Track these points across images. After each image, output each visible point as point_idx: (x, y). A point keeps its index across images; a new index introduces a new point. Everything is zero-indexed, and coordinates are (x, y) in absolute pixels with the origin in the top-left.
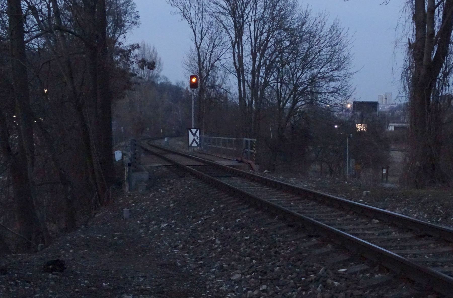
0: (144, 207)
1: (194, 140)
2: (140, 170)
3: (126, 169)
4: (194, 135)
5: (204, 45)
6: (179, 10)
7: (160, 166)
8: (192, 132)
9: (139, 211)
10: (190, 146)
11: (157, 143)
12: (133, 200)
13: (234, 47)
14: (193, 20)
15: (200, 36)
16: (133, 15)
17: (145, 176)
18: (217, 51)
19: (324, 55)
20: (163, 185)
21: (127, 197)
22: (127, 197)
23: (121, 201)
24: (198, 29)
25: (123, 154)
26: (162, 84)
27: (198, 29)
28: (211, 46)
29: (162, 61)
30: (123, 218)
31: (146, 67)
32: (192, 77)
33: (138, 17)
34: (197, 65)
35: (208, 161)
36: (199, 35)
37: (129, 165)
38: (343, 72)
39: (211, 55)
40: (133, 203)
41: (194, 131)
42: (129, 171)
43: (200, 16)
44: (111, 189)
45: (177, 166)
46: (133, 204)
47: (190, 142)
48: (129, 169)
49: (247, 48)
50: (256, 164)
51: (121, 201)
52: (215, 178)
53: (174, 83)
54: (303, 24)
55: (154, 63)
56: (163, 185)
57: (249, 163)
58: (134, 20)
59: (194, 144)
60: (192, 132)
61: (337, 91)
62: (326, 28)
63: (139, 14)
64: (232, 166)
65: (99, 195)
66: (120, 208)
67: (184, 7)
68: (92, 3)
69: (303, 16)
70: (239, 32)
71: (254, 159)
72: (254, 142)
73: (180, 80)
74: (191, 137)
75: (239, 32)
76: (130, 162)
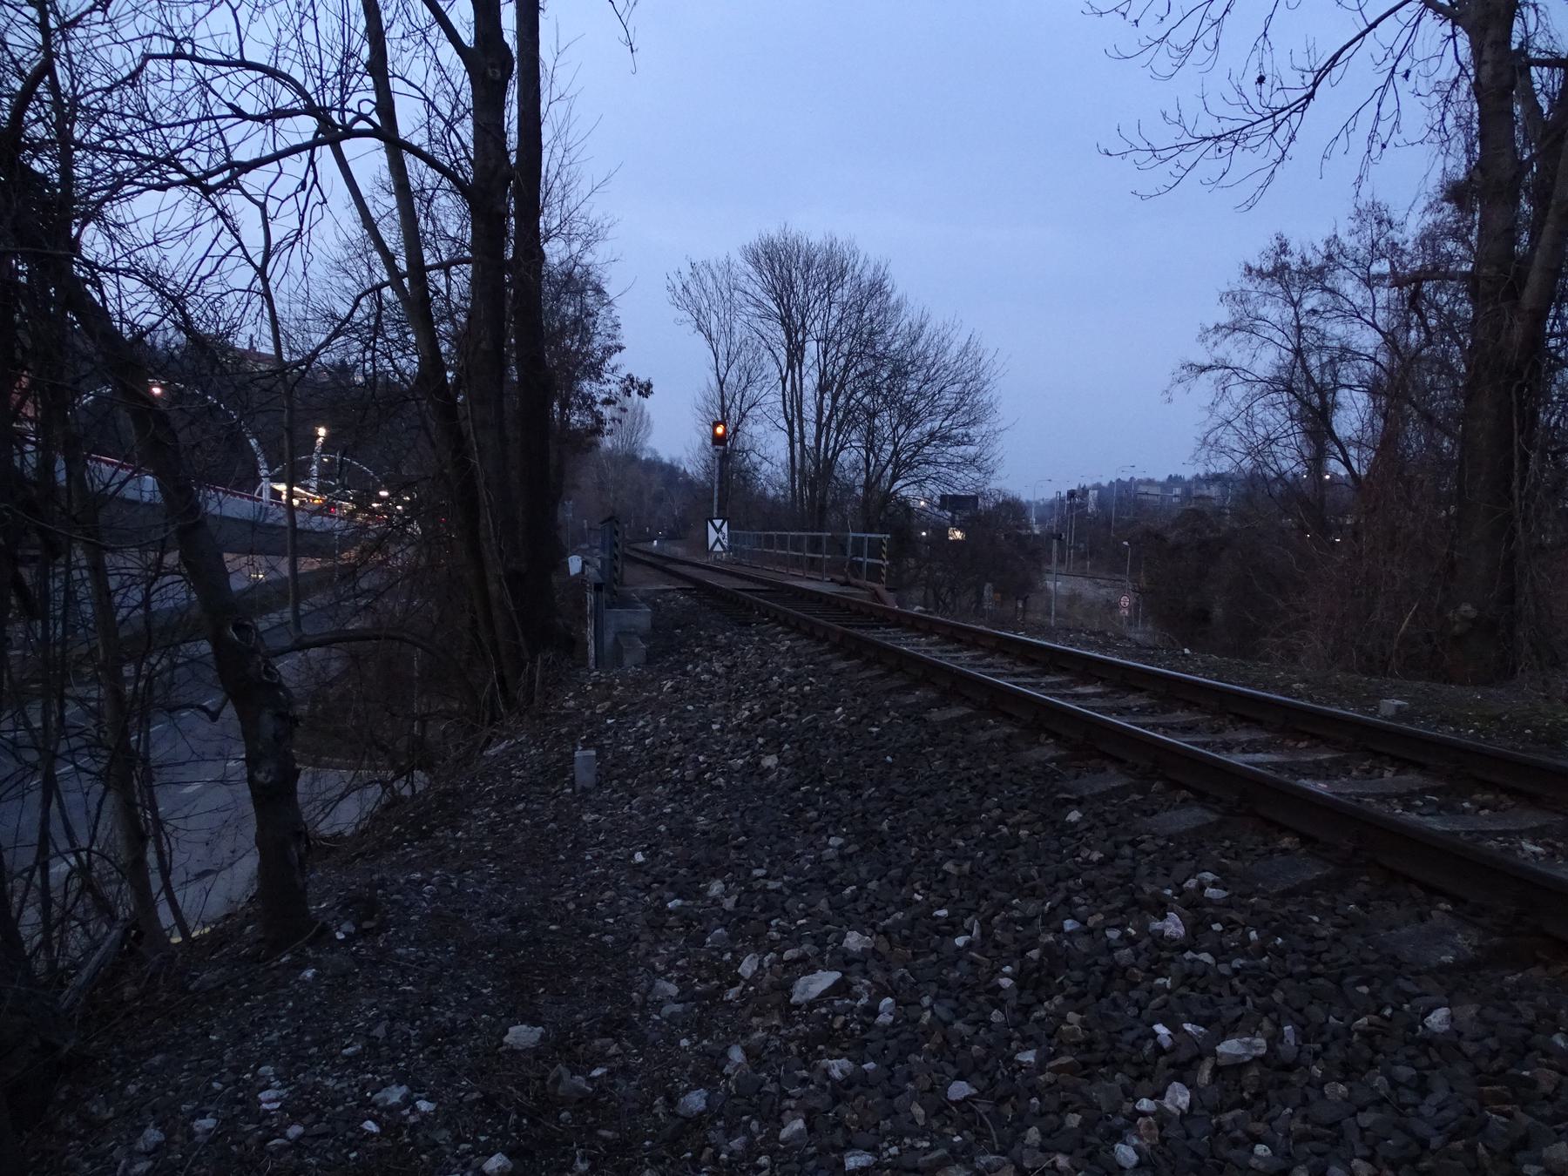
0: (647, 741)
1: (718, 540)
2: (625, 602)
3: (590, 597)
4: (718, 530)
5: (732, 378)
6: (689, 316)
7: (670, 590)
8: (713, 525)
9: (629, 754)
10: (709, 552)
11: (641, 546)
12: (607, 704)
14: (714, 335)
15: (725, 363)
16: (609, 323)
17: (641, 618)
18: (753, 392)
19: (949, 398)
20: (697, 650)
21: (589, 688)
22: (589, 688)
23: (572, 703)
24: (722, 350)
25: (585, 563)
26: (648, 460)
27: (722, 350)
28: (744, 380)
29: (652, 418)
30: (572, 782)
31: (634, 393)
32: (716, 424)
33: (618, 326)
34: (718, 411)
36: (723, 362)
37: (598, 587)
38: (984, 427)
39: (743, 396)
40: (609, 713)
41: (718, 523)
42: (596, 603)
43: (727, 329)
45: (713, 591)
46: (609, 721)
47: (711, 544)
48: (596, 598)
49: (810, 382)
50: (888, 589)
51: (572, 703)
52: (855, 631)
53: (666, 460)
54: (914, 341)
55: (650, 385)
56: (697, 650)
57: (873, 589)
58: (610, 331)
59: (718, 548)
60: (713, 525)
61: (971, 462)
62: (954, 351)
63: (620, 321)
64: (743, 590)
65: (502, 680)
66: (564, 731)
67: (699, 311)
68: (494, 72)
69: (915, 327)
70: (795, 353)
74: (712, 535)
75: (795, 353)
76: (599, 579)
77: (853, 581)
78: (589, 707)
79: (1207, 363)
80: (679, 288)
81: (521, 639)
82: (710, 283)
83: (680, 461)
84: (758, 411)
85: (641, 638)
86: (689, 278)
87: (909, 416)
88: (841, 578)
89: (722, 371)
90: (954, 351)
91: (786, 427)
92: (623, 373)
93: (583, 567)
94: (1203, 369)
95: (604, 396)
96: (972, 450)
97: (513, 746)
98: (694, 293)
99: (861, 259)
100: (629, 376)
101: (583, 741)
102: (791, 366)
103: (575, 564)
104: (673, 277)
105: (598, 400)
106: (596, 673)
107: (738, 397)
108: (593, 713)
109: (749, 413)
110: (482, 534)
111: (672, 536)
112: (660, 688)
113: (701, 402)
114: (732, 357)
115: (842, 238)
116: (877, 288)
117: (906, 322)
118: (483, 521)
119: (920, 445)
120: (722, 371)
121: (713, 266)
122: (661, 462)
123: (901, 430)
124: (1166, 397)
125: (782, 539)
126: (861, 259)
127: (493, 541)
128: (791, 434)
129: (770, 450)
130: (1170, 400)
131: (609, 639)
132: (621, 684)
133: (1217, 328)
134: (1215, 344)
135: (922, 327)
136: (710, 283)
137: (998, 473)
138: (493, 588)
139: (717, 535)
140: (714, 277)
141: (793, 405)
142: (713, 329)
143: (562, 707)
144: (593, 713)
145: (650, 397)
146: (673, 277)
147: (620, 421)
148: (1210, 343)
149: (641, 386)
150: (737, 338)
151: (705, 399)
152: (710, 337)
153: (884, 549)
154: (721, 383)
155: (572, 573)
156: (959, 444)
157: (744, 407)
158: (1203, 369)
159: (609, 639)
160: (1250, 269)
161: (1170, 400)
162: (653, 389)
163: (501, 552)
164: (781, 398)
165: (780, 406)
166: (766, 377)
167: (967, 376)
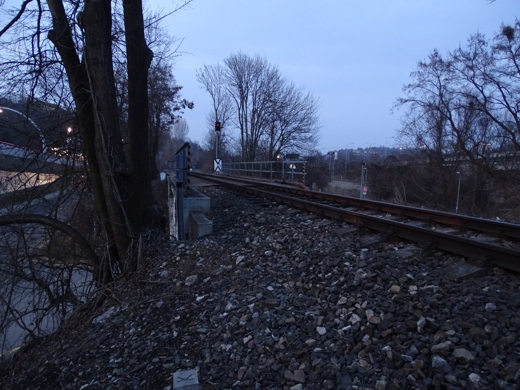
1: (218, 167)
4: (218, 163)
5: (220, 108)
7: (209, 186)
8: (216, 161)
13: (239, 110)
14: (213, 93)
17: (205, 203)
21: (178, 258)
22: (178, 258)
24: (216, 98)
25: (167, 175)
27: (216, 98)
28: (225, 109)
29: (189, 126)
31: (186, 107)
35: (235, 183)
36: (217, 103)
40: (197, 287)
41: (218, 160)
44: (140, 239)
53: (193, 142)
55: (193, 104)
59: (218, 170)
60: (216, 161)
62: (302, 98)
67: (208, 83)
70: (244, 98)
71: (303, 181)
72: (304, 164)
73: (197, 140)
74: (216, 165)
75: (244, 98)
77: (287, 181)
78: (179, 278)
79: (407, 98)
80: (201, 75)
81: (127, 223)
82: (212, 74)
83: (198, 142)
84: (230, 120)
85: (206, 214)
86: (204, 71)
87: (286, 123)
88: (282, 181)
89: (217, 106)
90: (302, 98)
91: (240, 127)
92: (182, 99)
93: (166, 177)
94: (406, 101)
95: (174, 107)
96: (308, 135)
97: (118, 315)
98: (206, 77)
99: (268, 64)
100: (184, 100)
101: (177, 323)
102: (242, 102)
103: (163, 176)
104: (198, 70)
105: (172, 108)
106: (182, 245)
107: (222, 116)
108: (183, 285)
109: (226, 122)
110: (97, 146)
111: (197, 168)
112: (233, 261)
113: (209, 117)
114: (220, 101)
115: (262, 56)
116: (273, 76)
117: (285, 87)
118: (97, 137)
119: (291, 132)
120: (217, 106)
121: (213, 67)
122: (191, 142)
123: (283, 127)
124: (391, 112)
125: (237, 168)
126: (268, 64)
127: (105, 151)
128: (242, 129)
129: (234, 135)
130: (393, 113)
131: (186, 215)
132: (201, 256)
133: (410, 86)
134: (409, 92)
135: (292, 89)
136: (212, 74)
137: (319, 143)
138: (106, 185)
139: (218, 165)
140: (213, 71)
141: (242, 119)
142: (213, 90)
143: (157, 276)
144: (183, 285)
145: (193, 109)
146: (198, 70)
147: (181, 117)
148: (407, 91)
149: (189, 104)
150: (221, 94)
151: (210, 116)
152: (212, 94)
153: (304, 167)
154: (216, 110)
155: (162, 179)
156: (305, 132)
157: (225, 119)
158: (406, 101)
159: (186, 215)
160: (421, 64)
161: (393, 113)
162: (194, 106)
163: (111, 159)
164: (238, 116)
165: (238, 119)
166: (232, 108)
167: (308, 107)
